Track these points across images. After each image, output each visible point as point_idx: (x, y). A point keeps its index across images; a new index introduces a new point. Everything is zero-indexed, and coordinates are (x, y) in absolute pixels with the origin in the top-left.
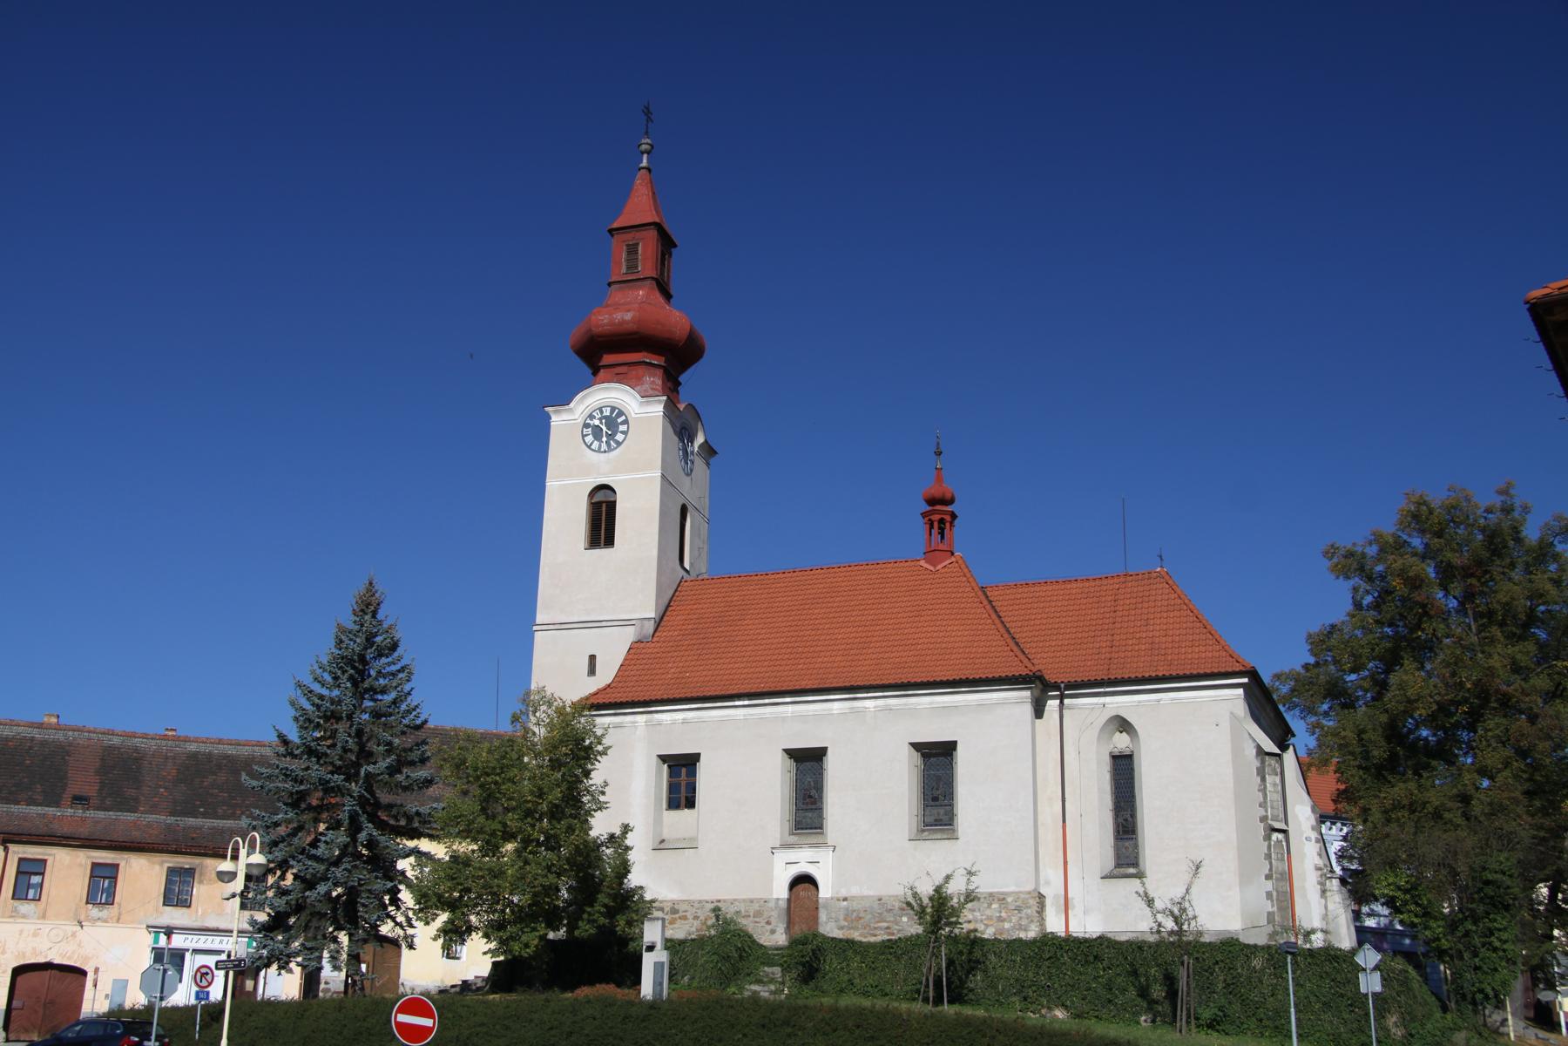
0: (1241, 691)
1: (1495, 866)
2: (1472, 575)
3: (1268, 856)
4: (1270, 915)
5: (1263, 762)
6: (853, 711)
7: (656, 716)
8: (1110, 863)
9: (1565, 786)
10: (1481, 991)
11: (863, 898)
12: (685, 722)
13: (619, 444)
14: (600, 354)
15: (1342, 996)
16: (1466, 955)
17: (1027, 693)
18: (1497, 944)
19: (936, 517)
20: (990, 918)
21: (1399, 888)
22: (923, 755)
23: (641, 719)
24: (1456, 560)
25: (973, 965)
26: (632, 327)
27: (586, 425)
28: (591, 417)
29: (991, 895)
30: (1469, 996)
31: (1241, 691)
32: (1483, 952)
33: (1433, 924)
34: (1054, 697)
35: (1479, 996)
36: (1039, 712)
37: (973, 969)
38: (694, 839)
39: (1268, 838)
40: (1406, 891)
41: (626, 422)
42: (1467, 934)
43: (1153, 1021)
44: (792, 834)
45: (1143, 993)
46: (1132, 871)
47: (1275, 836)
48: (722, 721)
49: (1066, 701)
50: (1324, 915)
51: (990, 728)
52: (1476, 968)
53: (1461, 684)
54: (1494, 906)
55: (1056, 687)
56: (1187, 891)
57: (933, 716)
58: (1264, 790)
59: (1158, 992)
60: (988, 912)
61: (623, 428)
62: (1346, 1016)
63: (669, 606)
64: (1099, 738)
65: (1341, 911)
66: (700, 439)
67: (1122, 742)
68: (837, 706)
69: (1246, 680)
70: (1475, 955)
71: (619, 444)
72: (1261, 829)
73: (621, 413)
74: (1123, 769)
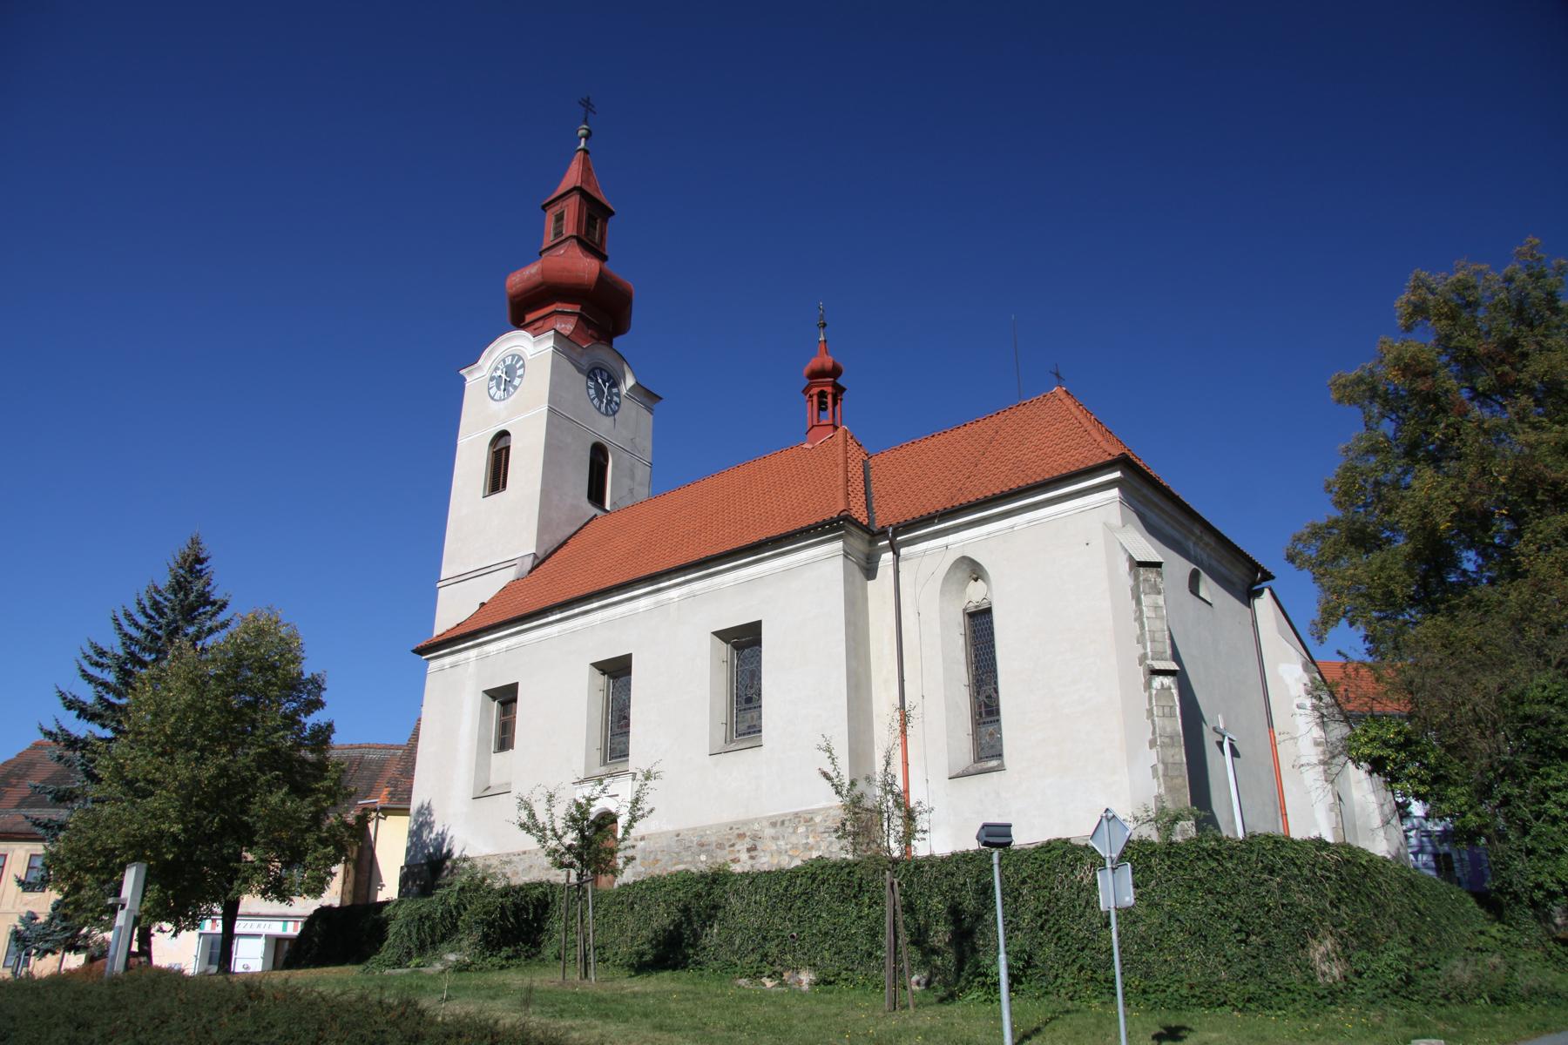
0: (1115, 492)
1: (1537, 693)
2: (1502, 362)
3: (1150, 712)
4: (1158, 798)
5: (1136, 578)
6: (660, 605)
7: (487, 648)
8: (965, 755)
9: (1566, 498)
10: (1539, 886)
11: (660, 835)
12: (508, 650)
13: (515, 388)
14: (524, 310)
15: (1224, 916)
16: (1512, 835)
17: (838, 545)
18: (1557, 811)
19: (815, 390)
20: (795, 847)
21: (1386, 743)
22: (737, 647)
23: (473, 653)
24: (1481, 348)
25: (712, 912)
26: (538, 279)
27: (492, 379)
28: (496, 369)
29: (797, 815)
30: (1525, 899)
31: (1115, 492)
32: (1539, 826)
33: (1451, 792)
34: (884, 550)
35: (1538, 895)
36: (870, 571)
37: (710, 917)
38: (509, 784)
39: (1148, 686)
40: (1400, 747)
41: (523, 366)
42: (1506, 801)
43: (928, 984)
44: (605, 763)
45: (919, 939)
46: (994, 763)
47: (1158, 681)
48: (539, 641)
49: (903, 551)
50: (1320, 796)
51: (796, 592)
52: (1530, 852)
53: (1495, 483)
54: (1544, 754)
55: (883, 533)
56: (888, 764)
57: (732, 594)
58: (1139, 618)
59: (940, 935)
60: (794, 839)
61: (520, 372)
62: (1230, 949)
63: (565, 543)
64: (942, 592)
65: (1372, 798)
66: (630, 381)
67: (975, 594)
68: (641, 604)
69: (1117, 474)
70: (1525, 831)
71: (515, 388)
72: (1140, 674)
73: (520, 358)
74: (980, 622)
